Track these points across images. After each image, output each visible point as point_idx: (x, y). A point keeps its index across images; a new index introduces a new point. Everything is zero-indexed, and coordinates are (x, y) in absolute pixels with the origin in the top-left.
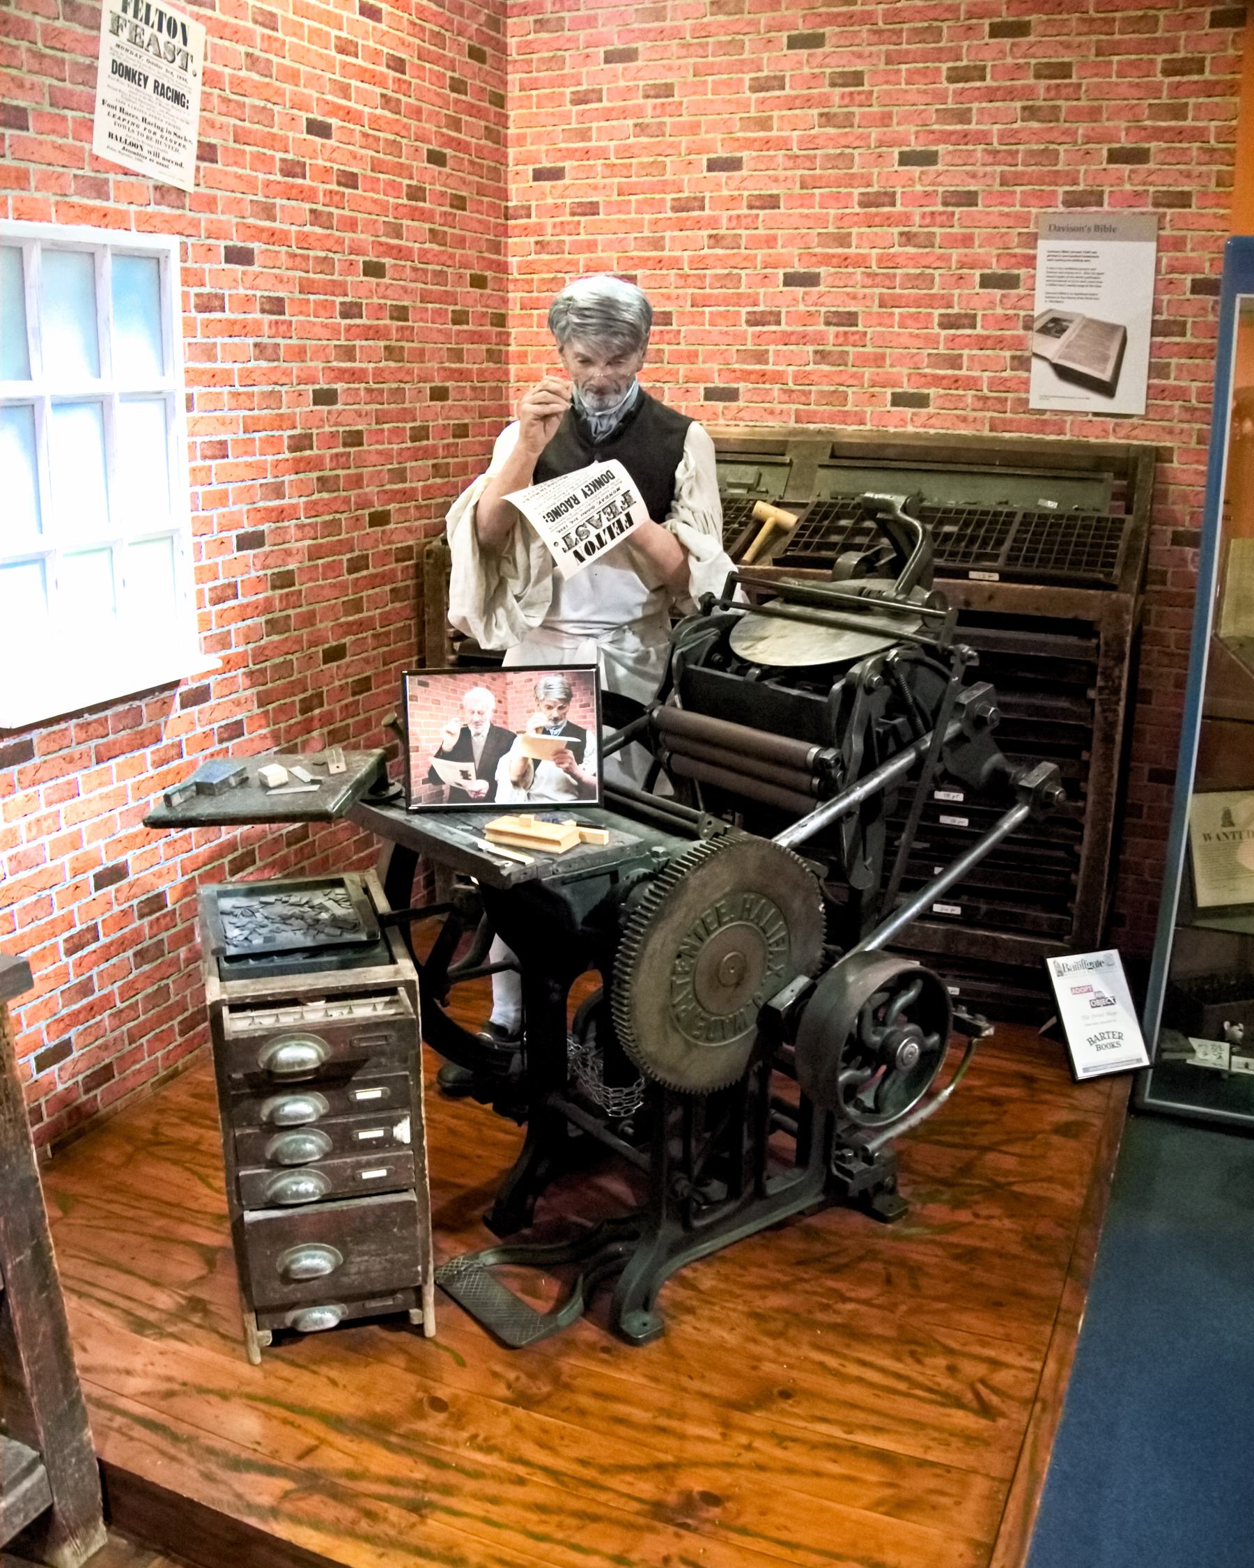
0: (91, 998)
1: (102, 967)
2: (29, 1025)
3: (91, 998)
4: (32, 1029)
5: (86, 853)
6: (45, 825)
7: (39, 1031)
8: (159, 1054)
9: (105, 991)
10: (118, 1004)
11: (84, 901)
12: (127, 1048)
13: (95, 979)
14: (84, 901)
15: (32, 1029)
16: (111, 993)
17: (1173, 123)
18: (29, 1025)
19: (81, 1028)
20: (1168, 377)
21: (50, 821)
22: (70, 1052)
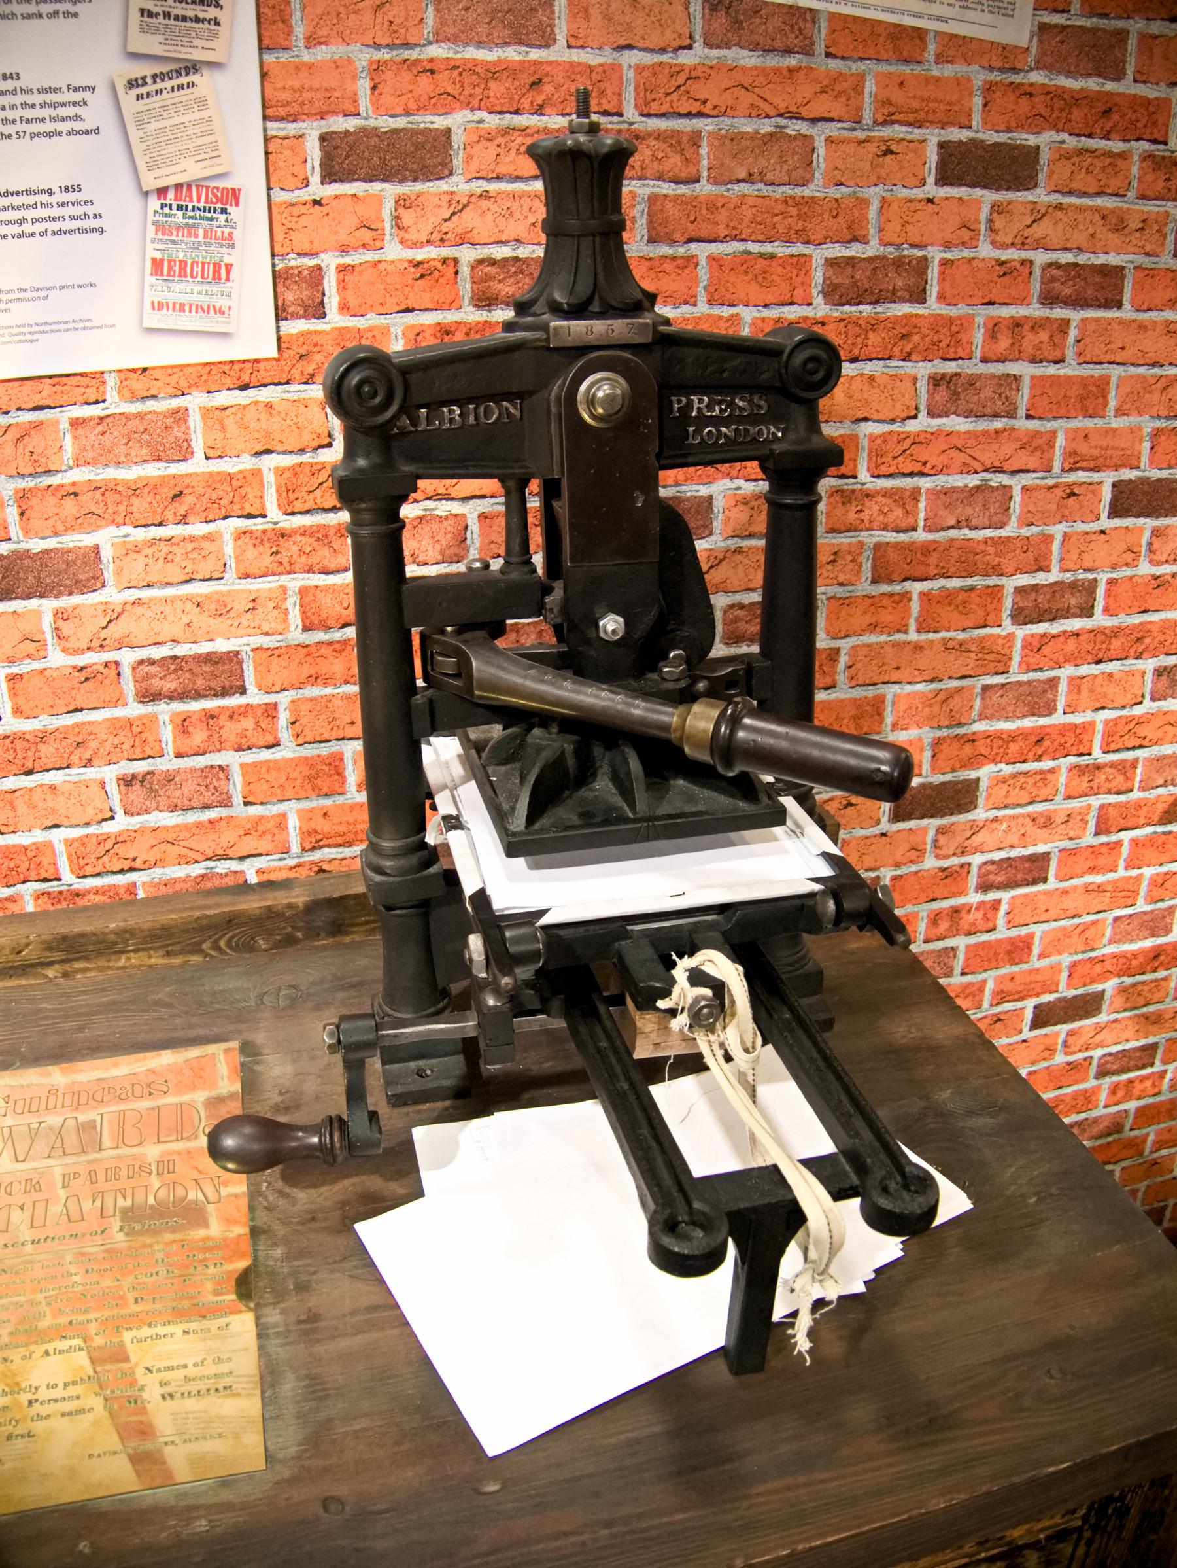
0: (1043, 721)
1: (1085, 670)
2: (1041, 956)
3: (1043, 721)
4: (1045, 962)
5: (1110, 432)
6: (1030, 340)
7: (1055, 969)
8: (1148, 872)
9: (1077, 719)
10: (1097, 752)
11: (1080, 527)
12: (1089, 839)
13: (1063, 687)
14: (1080, 527)
15: (1045, 962)
16: (1089, 727)
17: (512, 54)
18: (1041, 956)
19: (1007, 769)
20: (548, 41)
21: (1044, 336)
22: (1097, 1010)
